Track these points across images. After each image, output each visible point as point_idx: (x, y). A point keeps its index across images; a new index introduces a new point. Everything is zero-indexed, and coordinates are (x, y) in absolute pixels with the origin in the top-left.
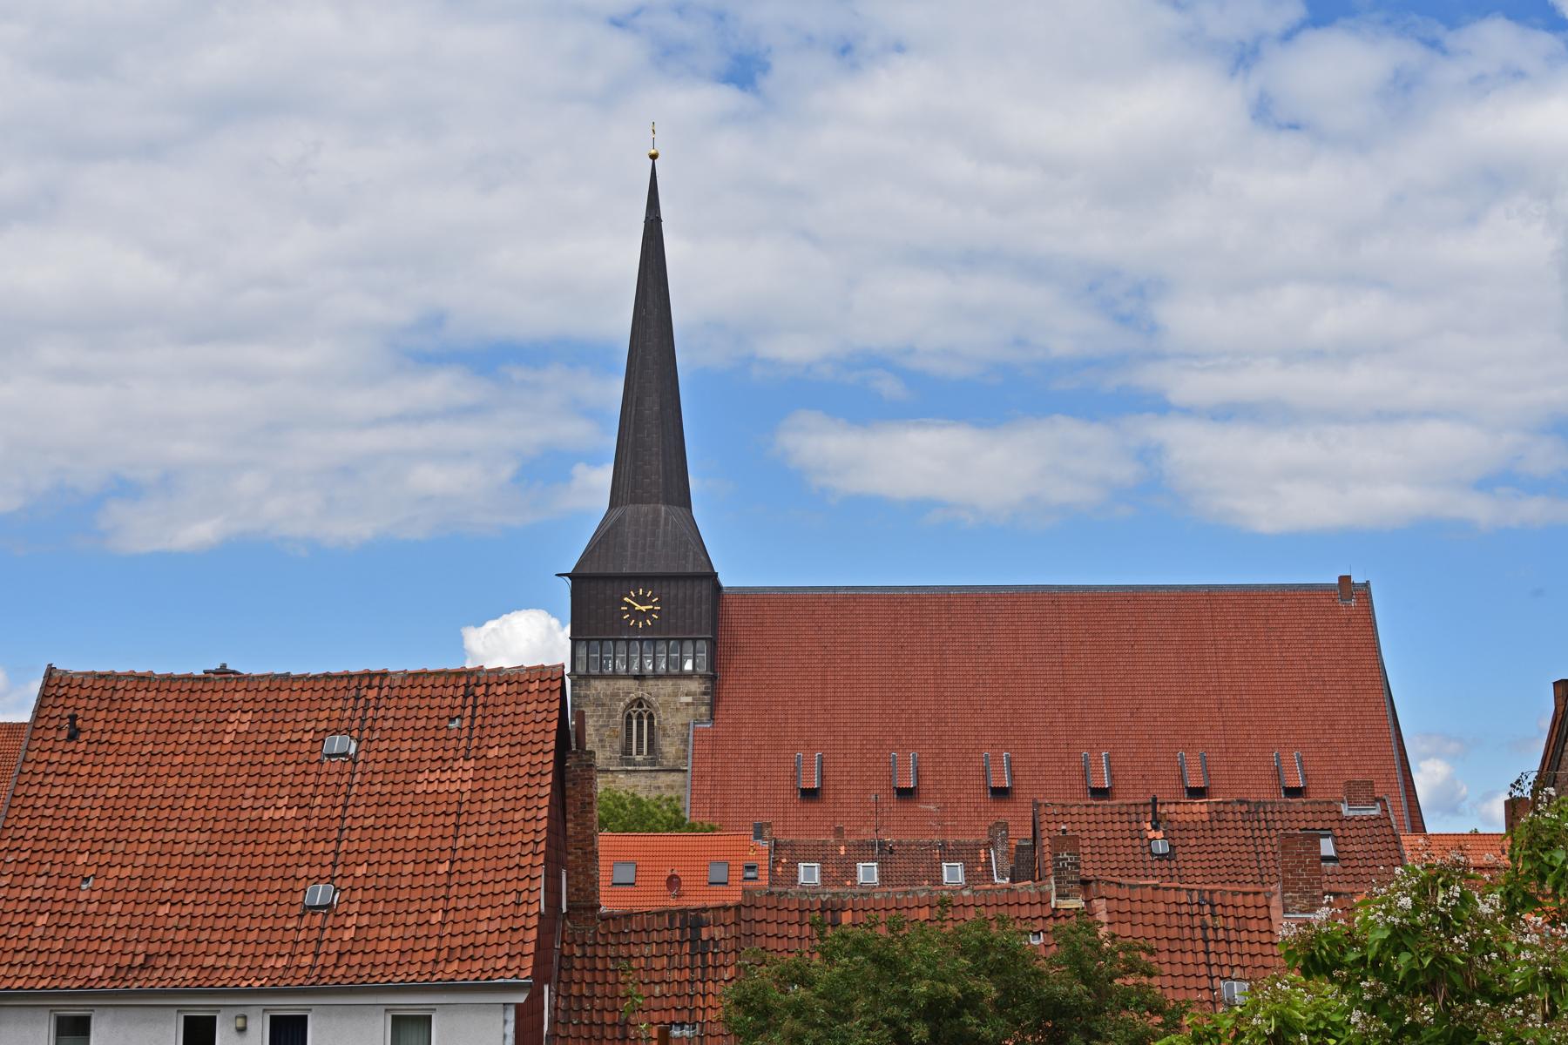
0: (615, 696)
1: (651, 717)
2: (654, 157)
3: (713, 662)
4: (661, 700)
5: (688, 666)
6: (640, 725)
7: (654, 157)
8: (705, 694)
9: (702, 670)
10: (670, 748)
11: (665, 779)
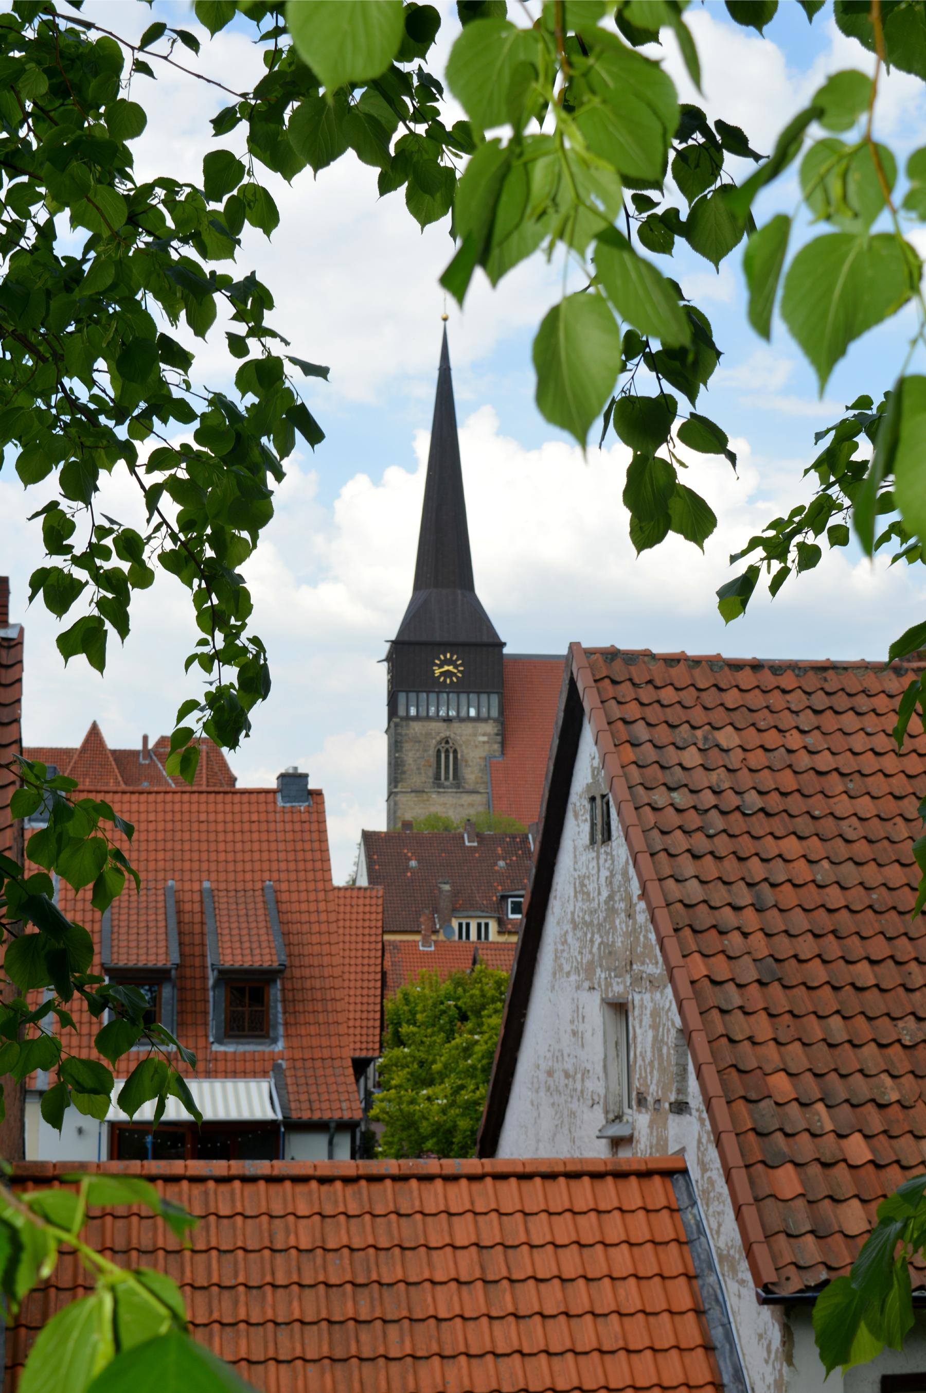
0: (428, 735)
1: (455, 752)
2: (445, 319)
3: (502, 711)
4: (464, 738)
5: (413, 712)
6: (447, 757)
7: (445, 319)
8: (497, 734)
9: (495, 713)
10: (471, 775)
11: (467, 799)
